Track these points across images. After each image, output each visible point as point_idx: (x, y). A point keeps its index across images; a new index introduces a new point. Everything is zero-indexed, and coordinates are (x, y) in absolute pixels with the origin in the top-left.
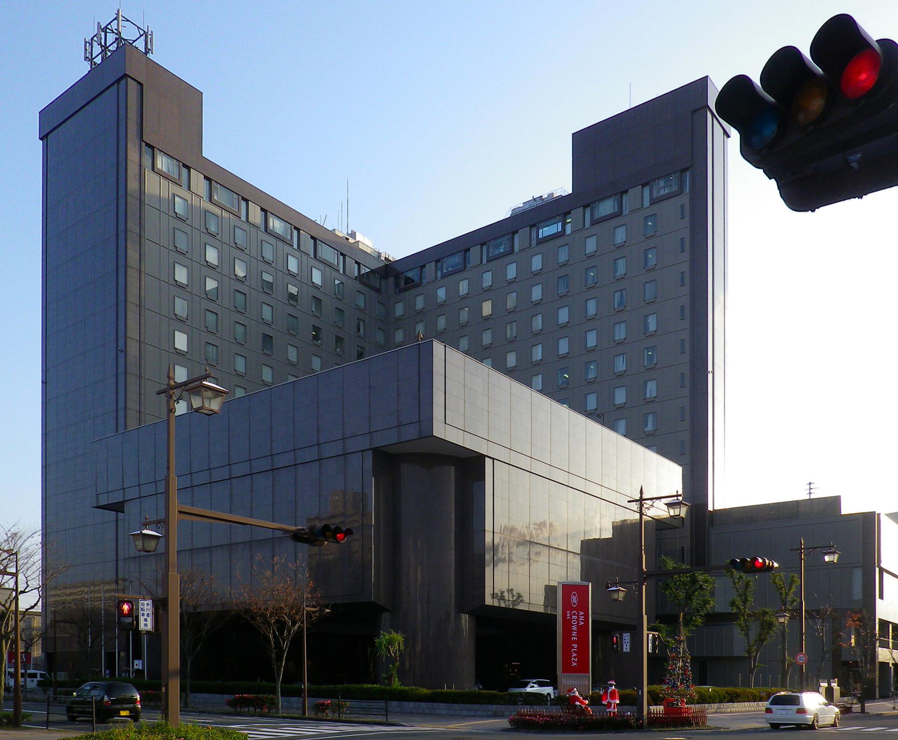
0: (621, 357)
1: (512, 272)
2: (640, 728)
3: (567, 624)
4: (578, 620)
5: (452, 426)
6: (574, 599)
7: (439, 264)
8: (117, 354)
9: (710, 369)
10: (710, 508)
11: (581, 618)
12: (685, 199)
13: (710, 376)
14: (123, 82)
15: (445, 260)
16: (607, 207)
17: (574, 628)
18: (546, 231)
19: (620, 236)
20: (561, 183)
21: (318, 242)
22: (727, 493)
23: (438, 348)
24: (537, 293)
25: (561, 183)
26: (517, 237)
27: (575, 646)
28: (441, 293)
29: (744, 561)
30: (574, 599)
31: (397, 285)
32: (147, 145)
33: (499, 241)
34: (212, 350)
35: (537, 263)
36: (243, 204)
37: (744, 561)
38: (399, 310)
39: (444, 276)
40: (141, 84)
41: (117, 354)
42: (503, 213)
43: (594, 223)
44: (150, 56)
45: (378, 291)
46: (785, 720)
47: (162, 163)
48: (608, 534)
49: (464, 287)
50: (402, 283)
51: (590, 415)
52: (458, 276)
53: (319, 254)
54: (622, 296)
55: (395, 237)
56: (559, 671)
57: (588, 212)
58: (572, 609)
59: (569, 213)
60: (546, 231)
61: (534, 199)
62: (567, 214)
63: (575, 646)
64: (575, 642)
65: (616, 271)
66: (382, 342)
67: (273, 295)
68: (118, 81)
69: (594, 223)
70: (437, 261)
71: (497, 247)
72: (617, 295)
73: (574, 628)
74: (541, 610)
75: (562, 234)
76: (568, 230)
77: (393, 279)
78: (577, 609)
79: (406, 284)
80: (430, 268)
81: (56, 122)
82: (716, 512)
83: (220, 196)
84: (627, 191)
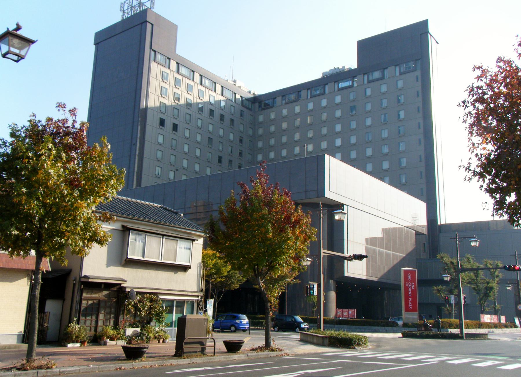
0: (386, 146)
1: (324, 103)
2: (461, 338)
3: (406, 288)
4: (411, 286)
5: (332, 192)
6: (409, 277)
7: (284, 98)
8: (131, 145)
9: (435, 153)
10: (439, 223)
11: (413, 286)
12: (418, 73)
13: (435, 157)
14: (144, 24)
15: (287, 96)
16: (377, 75)
17: (410, 290)
18: (342, 85)
19: (384, 88)
20: (351, 62)
21: (217, 84)
22: (448, 216)
23: (327, 157)
24: (338, 113)
25: (351, 62)
26: (327, 87)
27: (411, 299)
28: (285, 112)
29: (510, 266)
30: (409, 277)
31: (260, 106)
32: (153, 50)
33: (318, 88)
34: (174, 142)
35: (338, 99)
36: (168, 60)
37: (510, 266)
38: (261, 118)
39: (286, 104)
40: (152, 25)
41: (131, 145)
42: (318, 76)
43: (369, 82)
44: (153, 10)
45: (250, 109)
46: (158, 353)
47: (158, 56)
48: (380, 235)
49: (297, 109)
50: (263, 105)
51: (370, 173)
52: (295, 104)
53: (180, 71)
54: (385, 116)
55: (262, 88)
56: (403, 312)
57: (366, 76)
58: (408, 281)
59: (356, 76)
60: (342, 85)
61: (335, 69)
62: (355, 77)
63: (411, 299)
64: (410, 297)
65: (382, 104)
66: (242, 130)
67: (192, 109)
68: (142, 23)
69: (369, 82)
70: (283, 96)
71: (316, 91)
72: (383, 116)
73: (410, 290)
74: (364, 278)
75: (352, 86)
76: (355, 85)
77: (259, 103)
78: (411, 281)
79: (265, 106)
80: (279, 99)
81: (104, 39)
82: (442, 226)
83: (183, 70)
84: (387, 68)
